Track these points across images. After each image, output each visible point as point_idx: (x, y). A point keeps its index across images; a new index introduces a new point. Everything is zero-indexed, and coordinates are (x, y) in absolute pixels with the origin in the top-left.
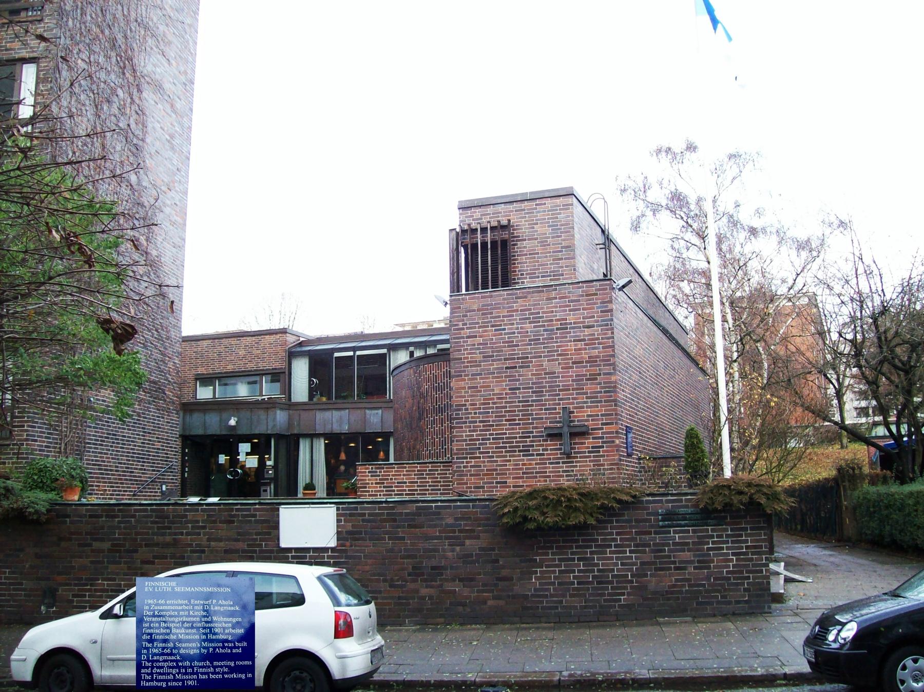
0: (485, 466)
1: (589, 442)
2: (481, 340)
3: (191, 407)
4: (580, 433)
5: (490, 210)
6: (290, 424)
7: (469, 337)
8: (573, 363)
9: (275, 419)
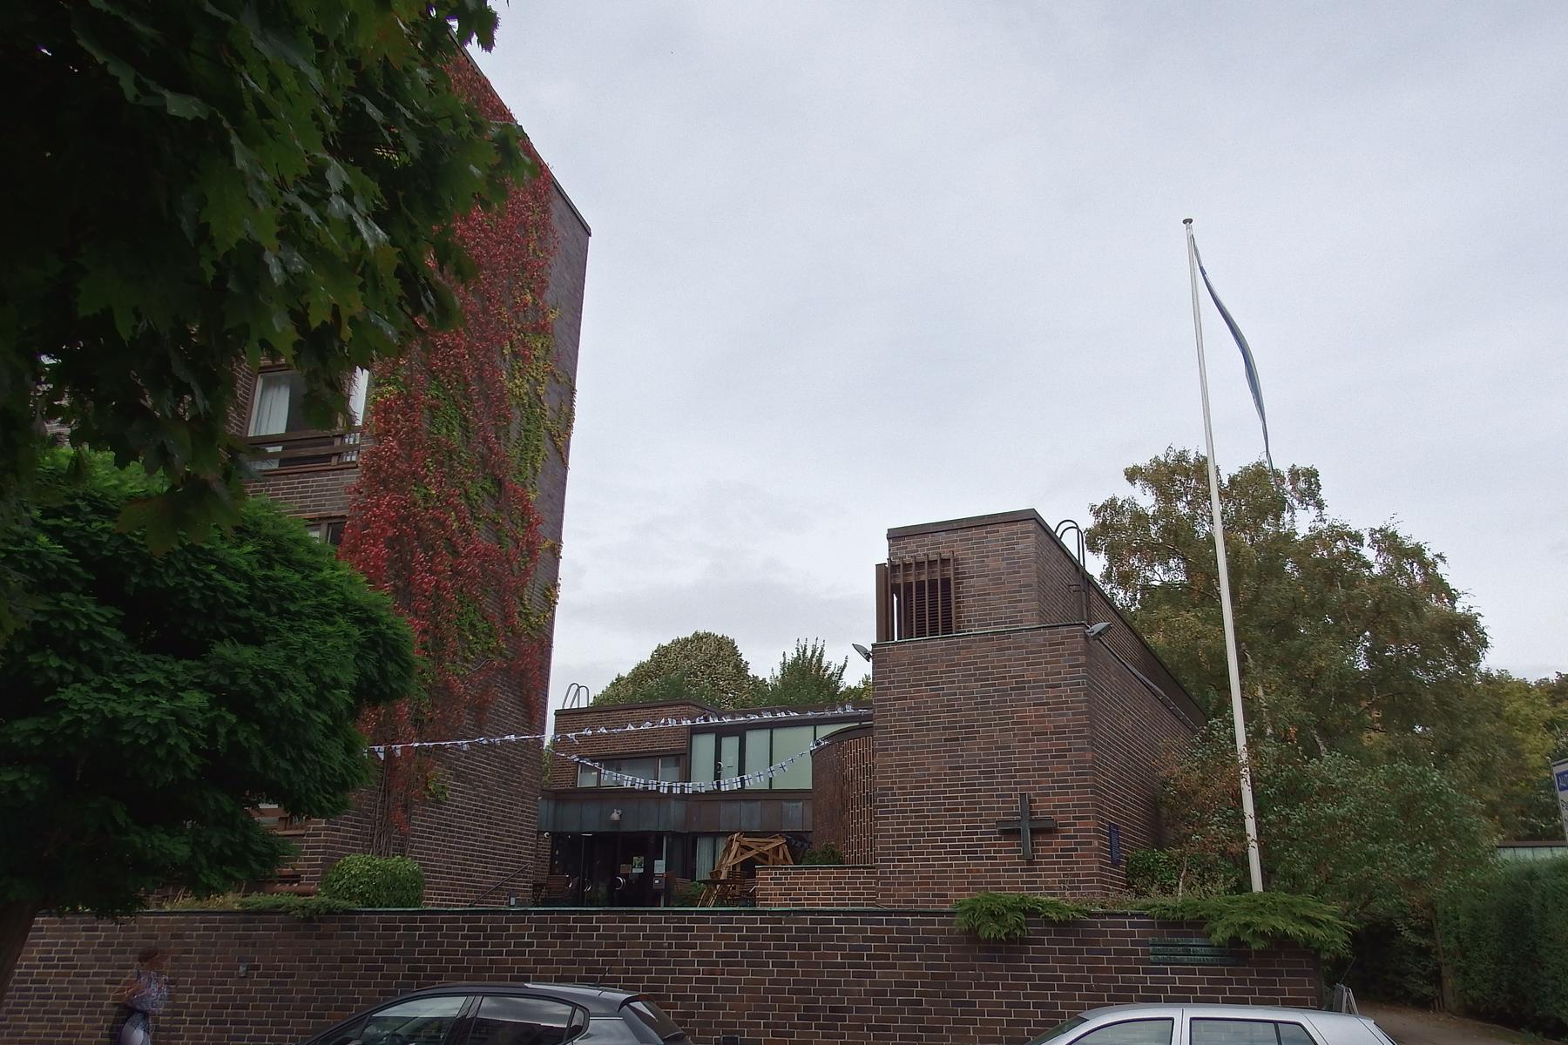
1: (1057, 842)
3: (566, 796)
4: (1045, 830)
5: (928, 540)
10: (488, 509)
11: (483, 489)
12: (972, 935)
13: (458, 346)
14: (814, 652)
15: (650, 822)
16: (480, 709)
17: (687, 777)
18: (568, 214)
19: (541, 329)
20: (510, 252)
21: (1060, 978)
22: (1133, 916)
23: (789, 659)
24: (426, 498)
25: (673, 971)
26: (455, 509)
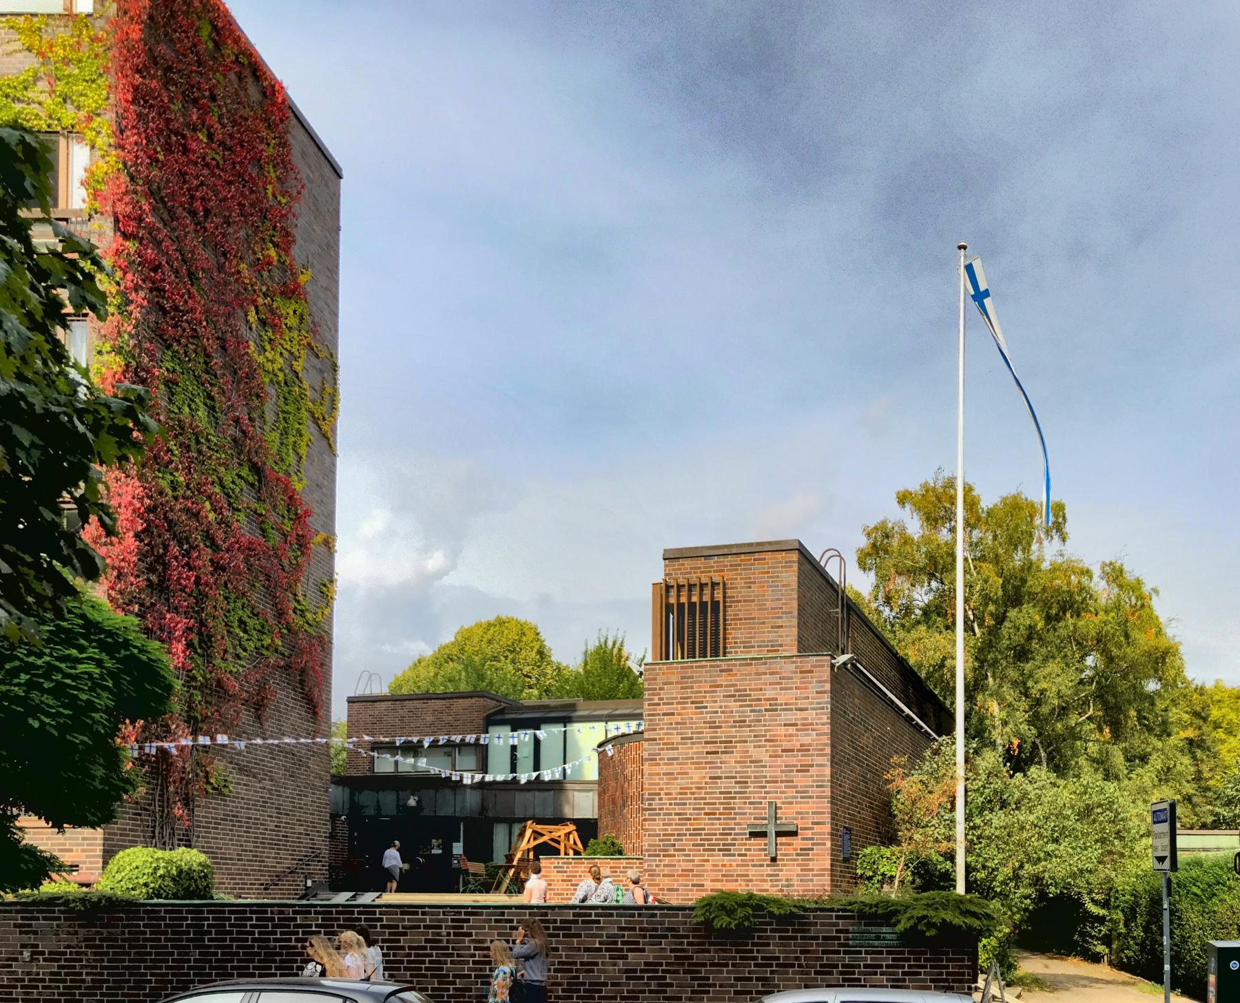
1: (797, 842)
2: (678, 718)
6: (483, 809)
7: (664, 714)
8: (783, 751)
9: (463, 801)
10: (247, 499)
11: (239, 476)
12: (708, 923)
13: (192, 310)
14: (614, 644)
15: (448, 806)
16: (258, 706)
17: (484, 769)
18: (312, 149)
19: (292, 292)
20: (245, 197)
21: (778, 958)
22: (838, 910)
24: (174, 486)
25: (451, 955)
26: (209, 498)
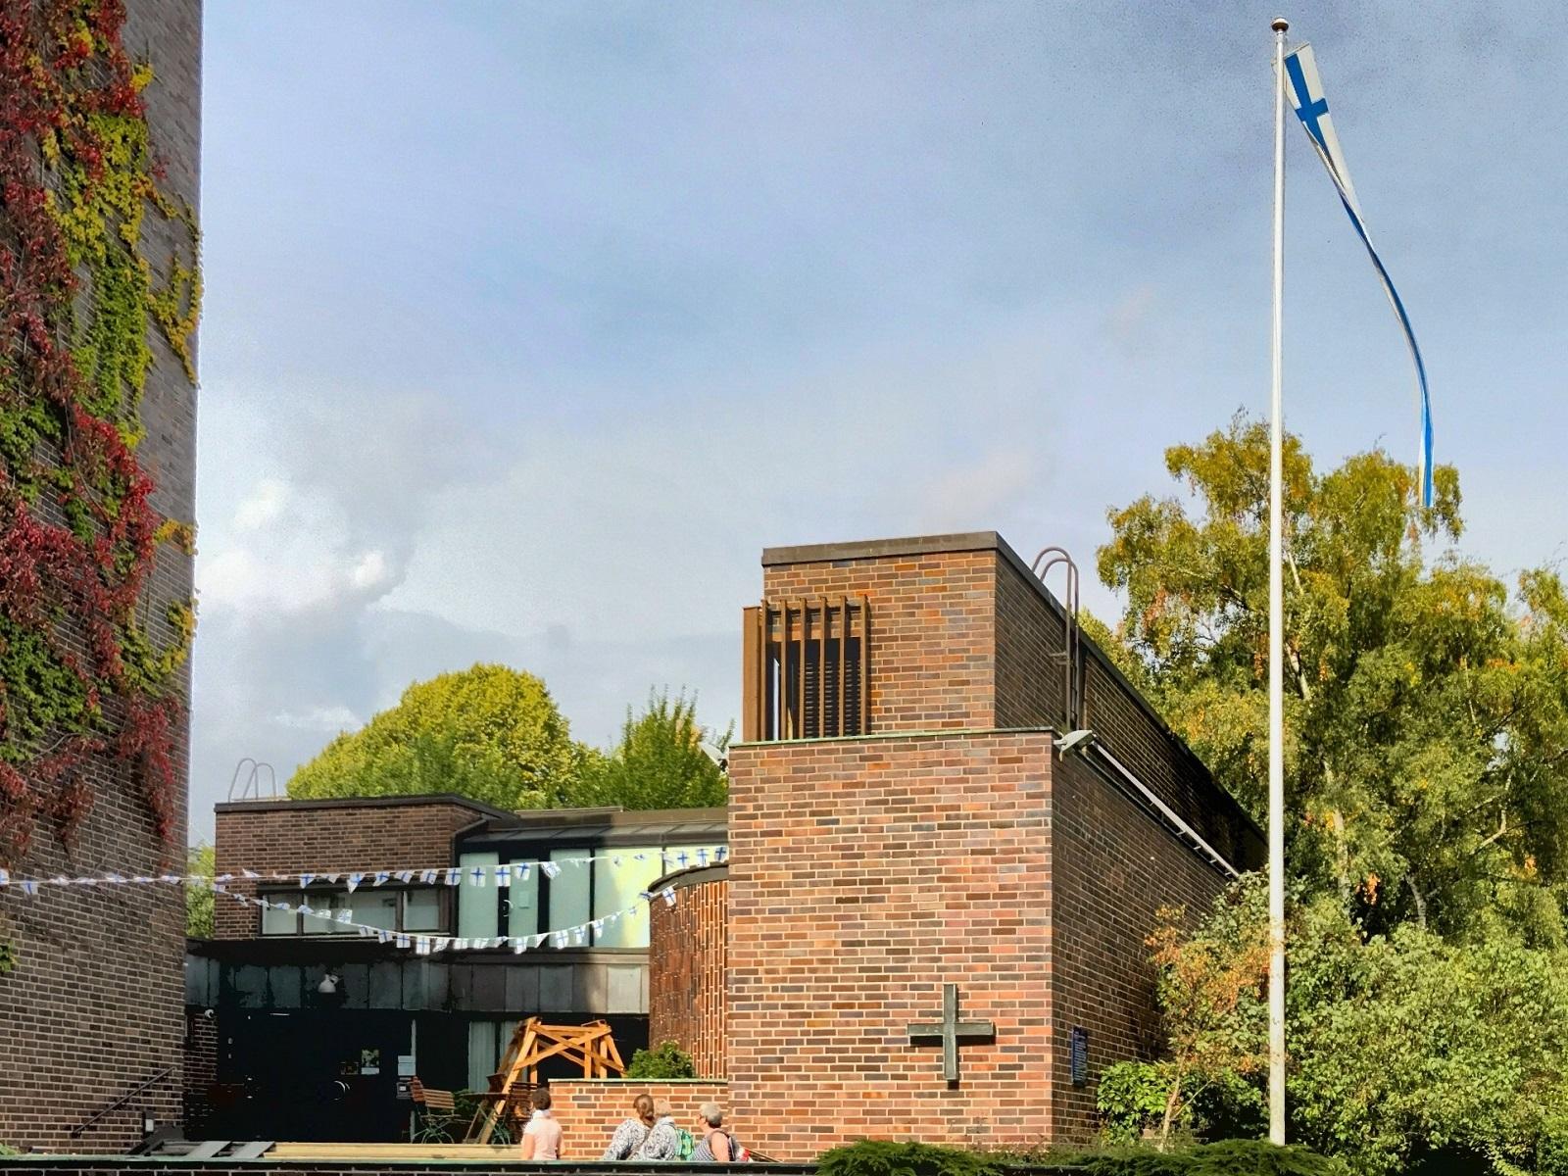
0: (791, 1096)
1: (994, 1055)
2: (789, 841)
9: (417, 983)
10: (42, 462)
11: (29, 423)
15: (389, 993)
19: (119, 104)
23: (638, 719)
